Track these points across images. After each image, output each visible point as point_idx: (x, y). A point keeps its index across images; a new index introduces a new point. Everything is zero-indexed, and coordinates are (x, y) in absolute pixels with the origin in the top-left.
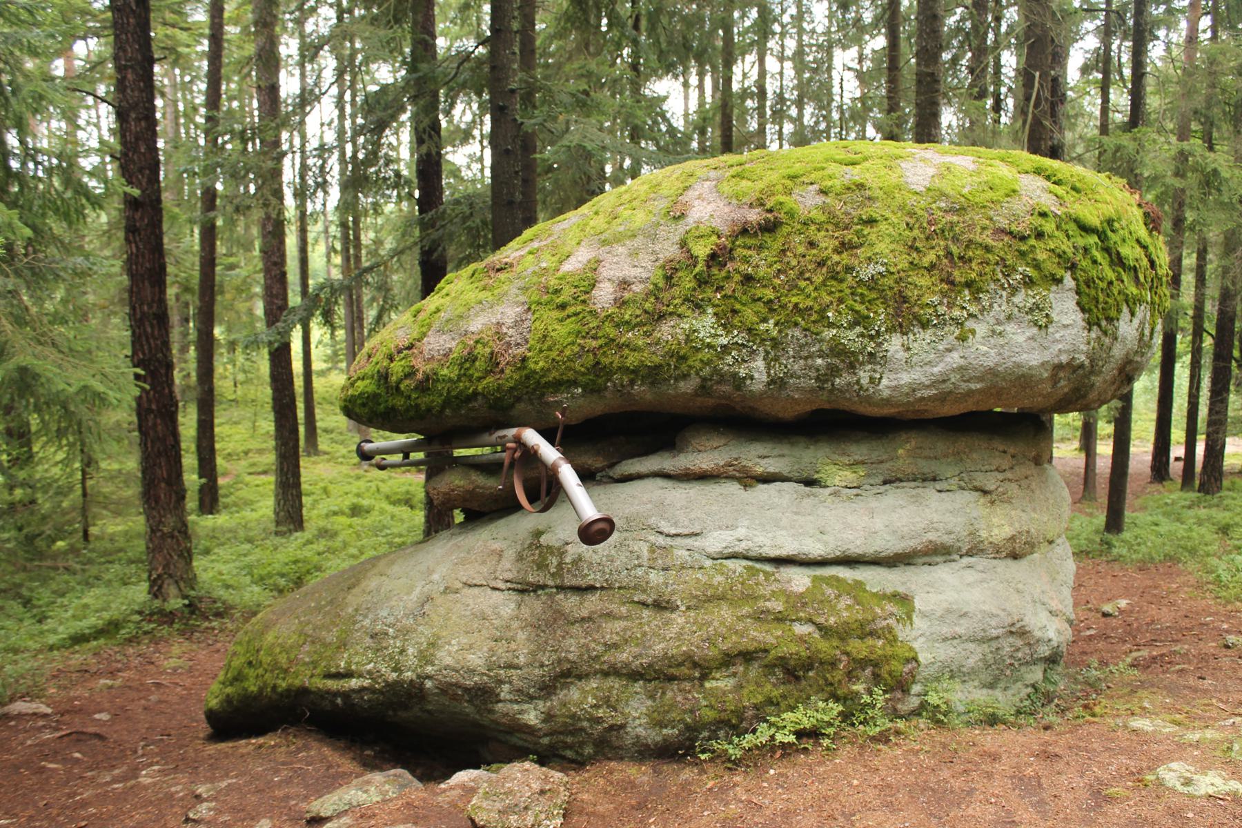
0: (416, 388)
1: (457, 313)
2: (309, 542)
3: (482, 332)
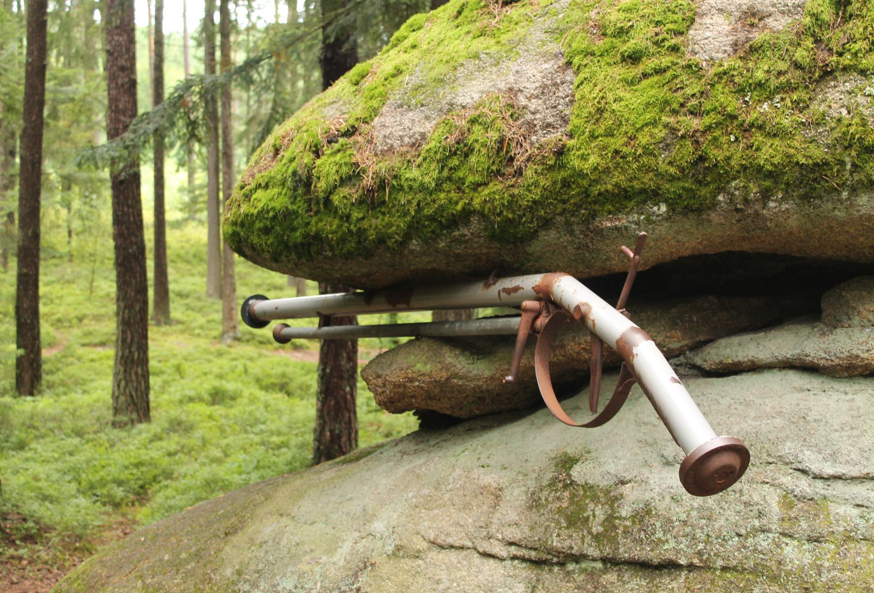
0: (361, 202)
1: (433, 74)
2: (157, 438)
3: (481, 104)
